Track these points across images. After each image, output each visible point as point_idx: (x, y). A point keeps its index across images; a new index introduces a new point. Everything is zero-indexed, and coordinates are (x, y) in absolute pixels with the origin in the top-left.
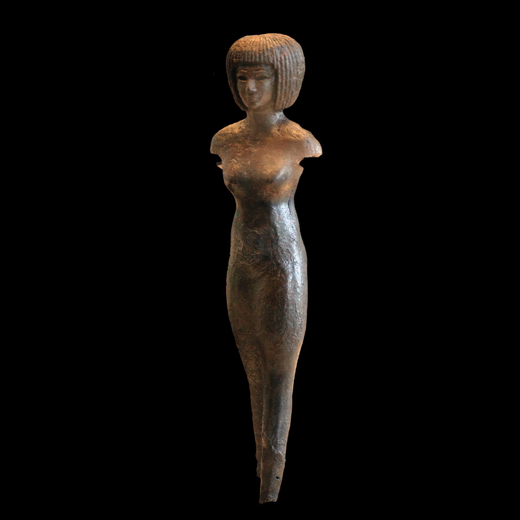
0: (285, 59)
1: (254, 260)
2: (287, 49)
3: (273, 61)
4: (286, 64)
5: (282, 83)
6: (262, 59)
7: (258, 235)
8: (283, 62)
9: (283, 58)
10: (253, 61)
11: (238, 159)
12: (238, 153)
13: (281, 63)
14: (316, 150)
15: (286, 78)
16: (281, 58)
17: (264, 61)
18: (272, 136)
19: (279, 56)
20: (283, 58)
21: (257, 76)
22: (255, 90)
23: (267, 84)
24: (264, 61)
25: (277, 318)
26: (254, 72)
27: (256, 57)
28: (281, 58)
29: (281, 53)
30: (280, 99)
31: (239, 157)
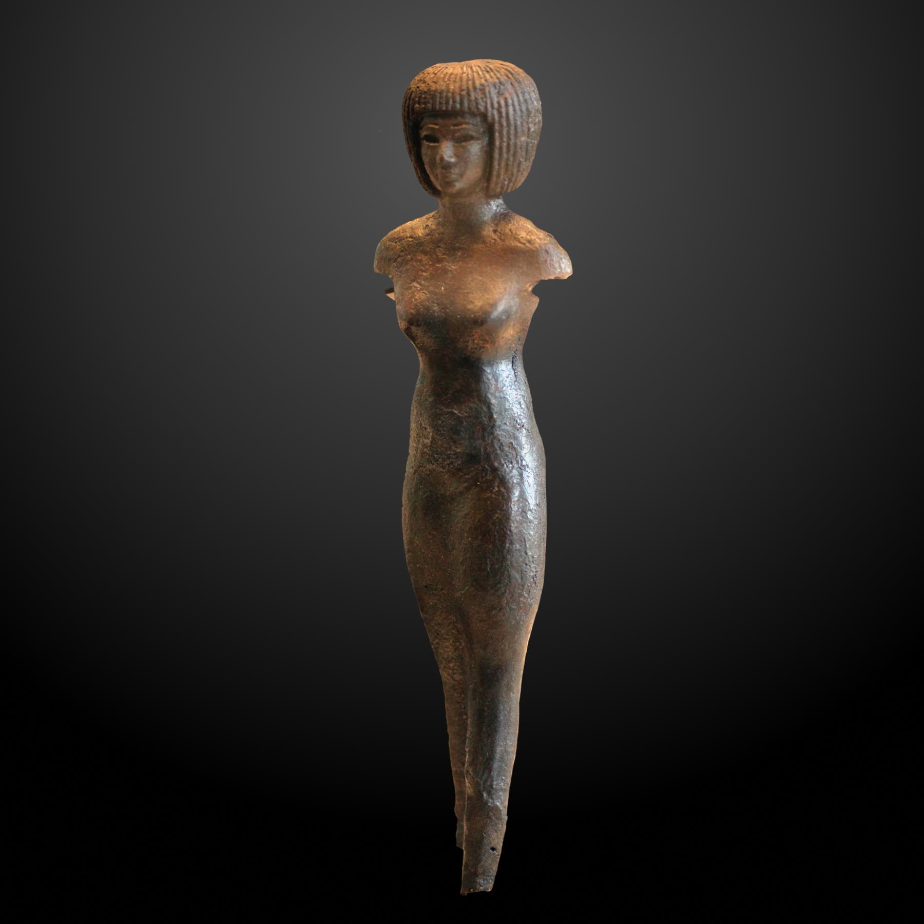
0: (507, 105)
1: (452, 463)
2: (509, 87)
3: (486, 108)
4: (507, 114)
5: (501, 148)
6: (466, 104)
7: (459, 418)
8: (503, 110)
9: (503, 103)
11: (423, 282)
12: (423, 271)
13: (500, 113)
14: (562, 267)
15: (509, 139)
16: (499, 103)
17: (469, 108)
18: (484, 242)
19: (495, 100)
20: (503, 103)
21: (457, 134)
22: (453, 160)
23: (475, 149)
24: (469, 108)
25: (492, 565)
26: (452, 128)
27: (454, 102)
28: (499, 103)
29: (499, 94)
30: (498, 176)
31: (426, 279)
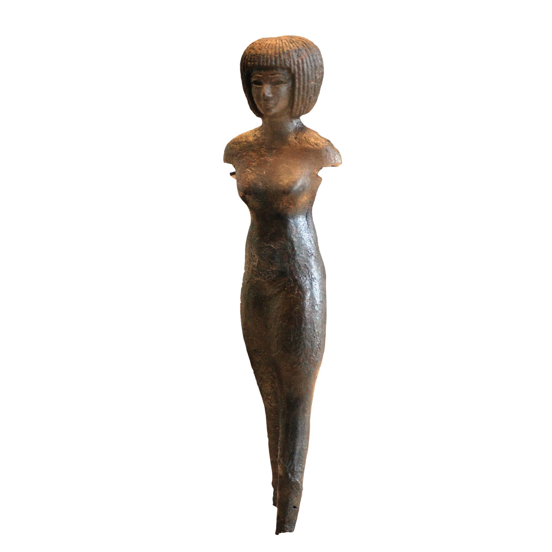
0: (303, 63)
1: (270, 276)
2: (304, 52)
3: (290, 64)
4: (303, 68)
5: (299, 89)
6: (278, 62)
7: (274, 249)
8: (301, 66)
9: (300, 61)
10: (269, 65)
11: (253, 169)
12: (253, 162)
13: (299, 67)
15: (304, 83)
16: (298, 61)
17: (280, 65)
18: (289, 145)
19: (296, 59)
20: (300, 61)
21: (273, 80)
22: (270, 96)
23: (284, 89)
24: (280, 65)
25: (294, 337)
26: (270, 76)
27: (271, 61)
28: (298, 61)
29: (298, 56)
30: (298, 105)
31: (254, 167)
